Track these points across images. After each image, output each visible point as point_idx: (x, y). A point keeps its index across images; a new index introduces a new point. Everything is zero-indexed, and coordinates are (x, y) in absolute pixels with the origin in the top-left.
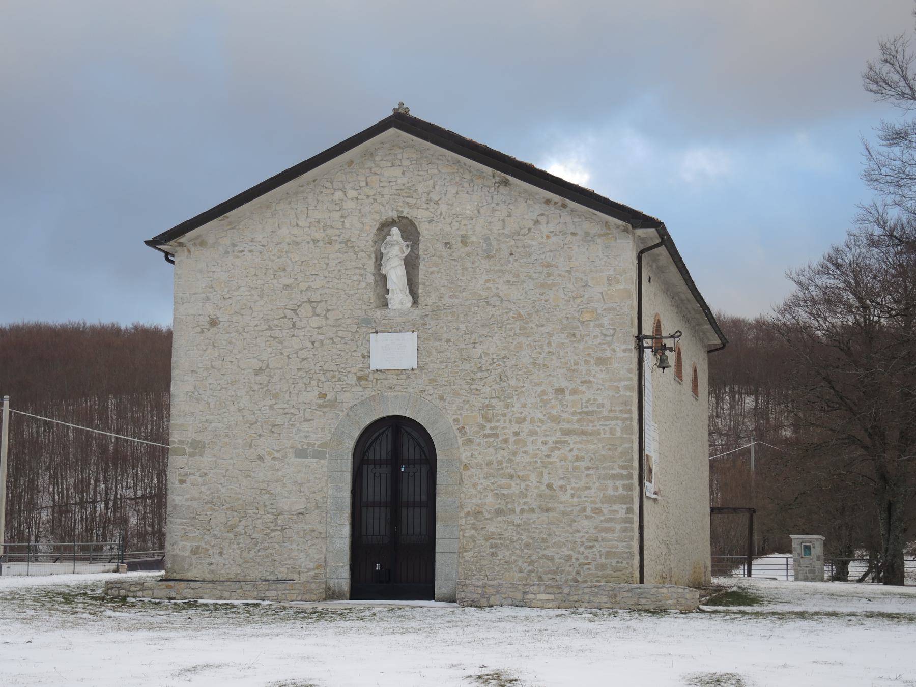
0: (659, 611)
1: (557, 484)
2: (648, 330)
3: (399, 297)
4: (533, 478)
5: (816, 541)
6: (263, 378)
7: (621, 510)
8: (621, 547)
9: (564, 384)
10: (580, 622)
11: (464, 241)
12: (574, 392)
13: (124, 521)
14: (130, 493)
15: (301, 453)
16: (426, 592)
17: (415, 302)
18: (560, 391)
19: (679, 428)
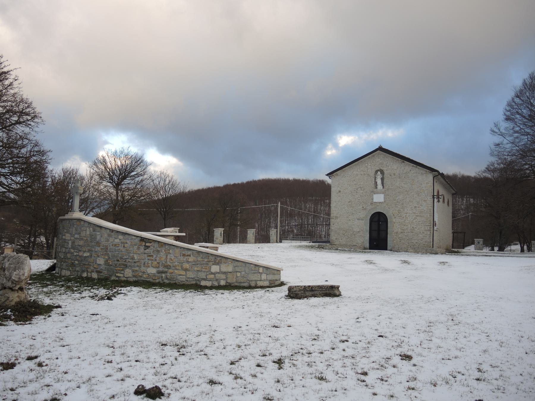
0: (436, 253)
1: (414, 227)
2: (435, 194)
3: (380, 186)
4: (409, 225)
5: (481, 240)
6: (350, 203)
7: (429, 233)
8: (428, 240)
9: (416, 205)
10: (419, 255)
11: (394, 174)
12: (419, 207)
13: (293, 231)
14: (294, 224)
15: (358, 219)
16: (386, 249)
17: (383, 187)
18: (415, 207)
19: (442, 215)
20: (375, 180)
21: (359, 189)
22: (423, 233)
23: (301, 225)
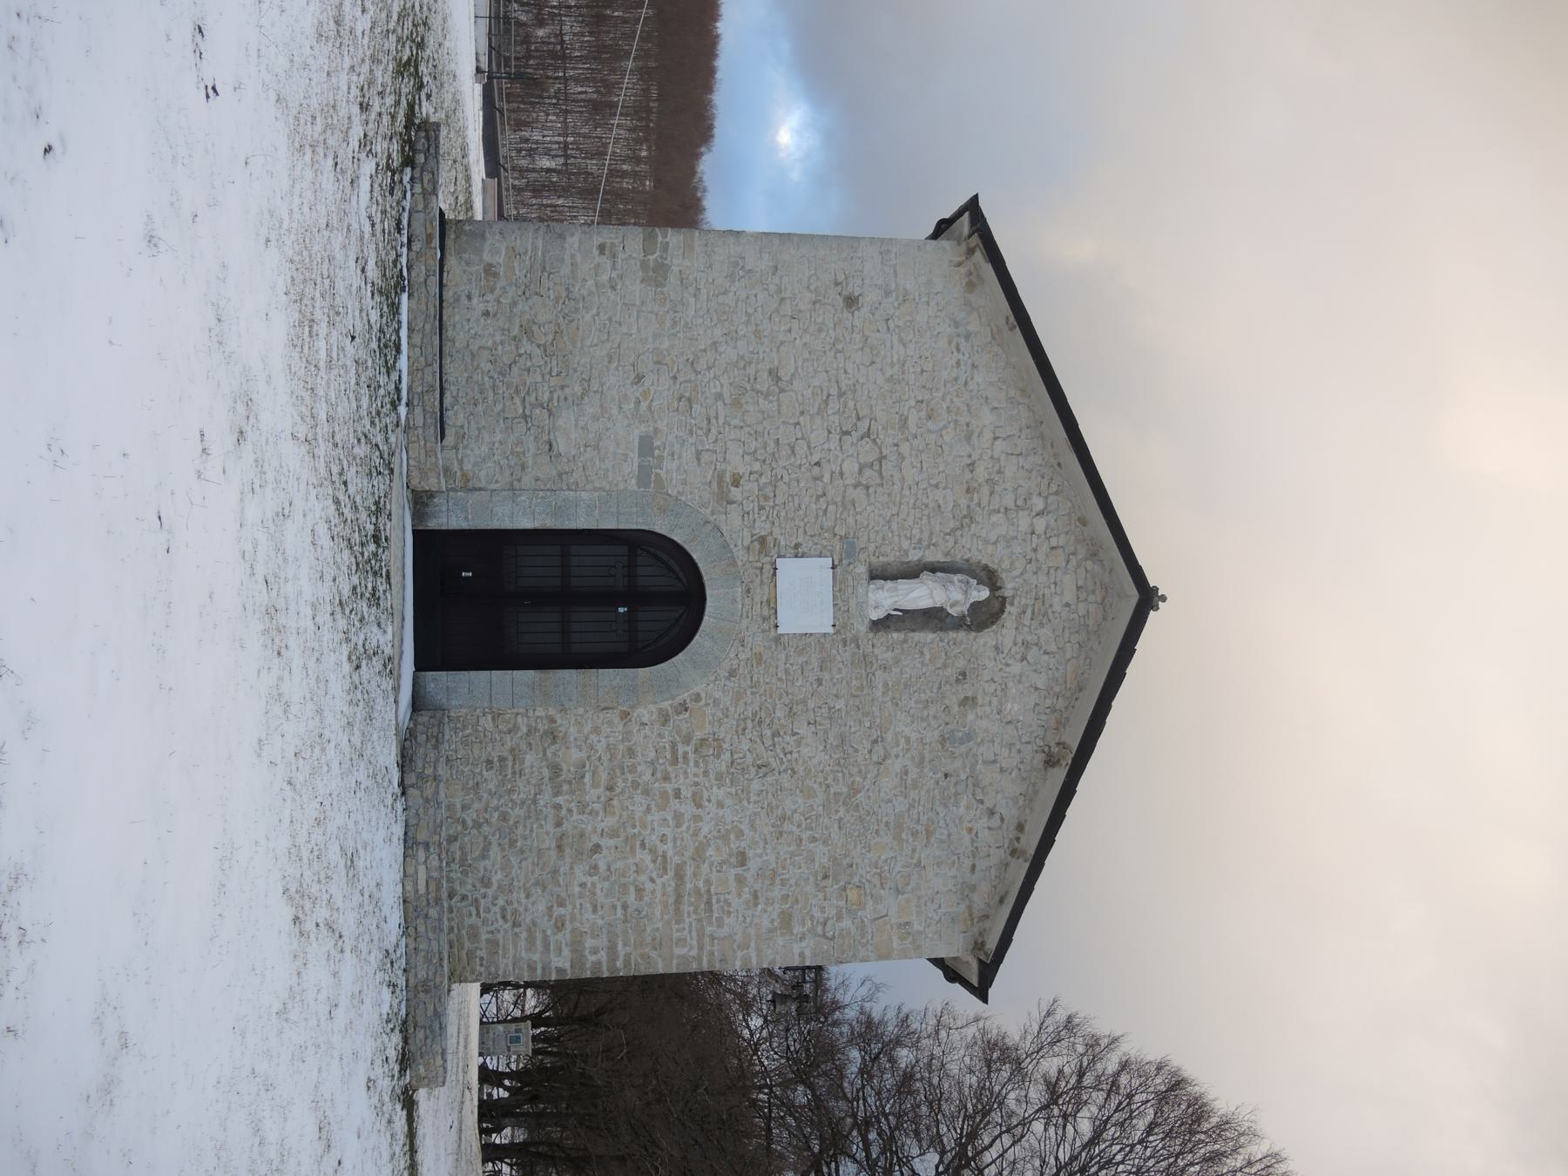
4: (611, 821)
6: (765, 383)
9: (753, 864)
11: (968, 702)
12: (740, 880)
13: (541, 23)
14: (566, 28)
18: (742, 859)
20: (934, 568)
21: (868, 452)
22: (560, 925)
23: (560, 56)
